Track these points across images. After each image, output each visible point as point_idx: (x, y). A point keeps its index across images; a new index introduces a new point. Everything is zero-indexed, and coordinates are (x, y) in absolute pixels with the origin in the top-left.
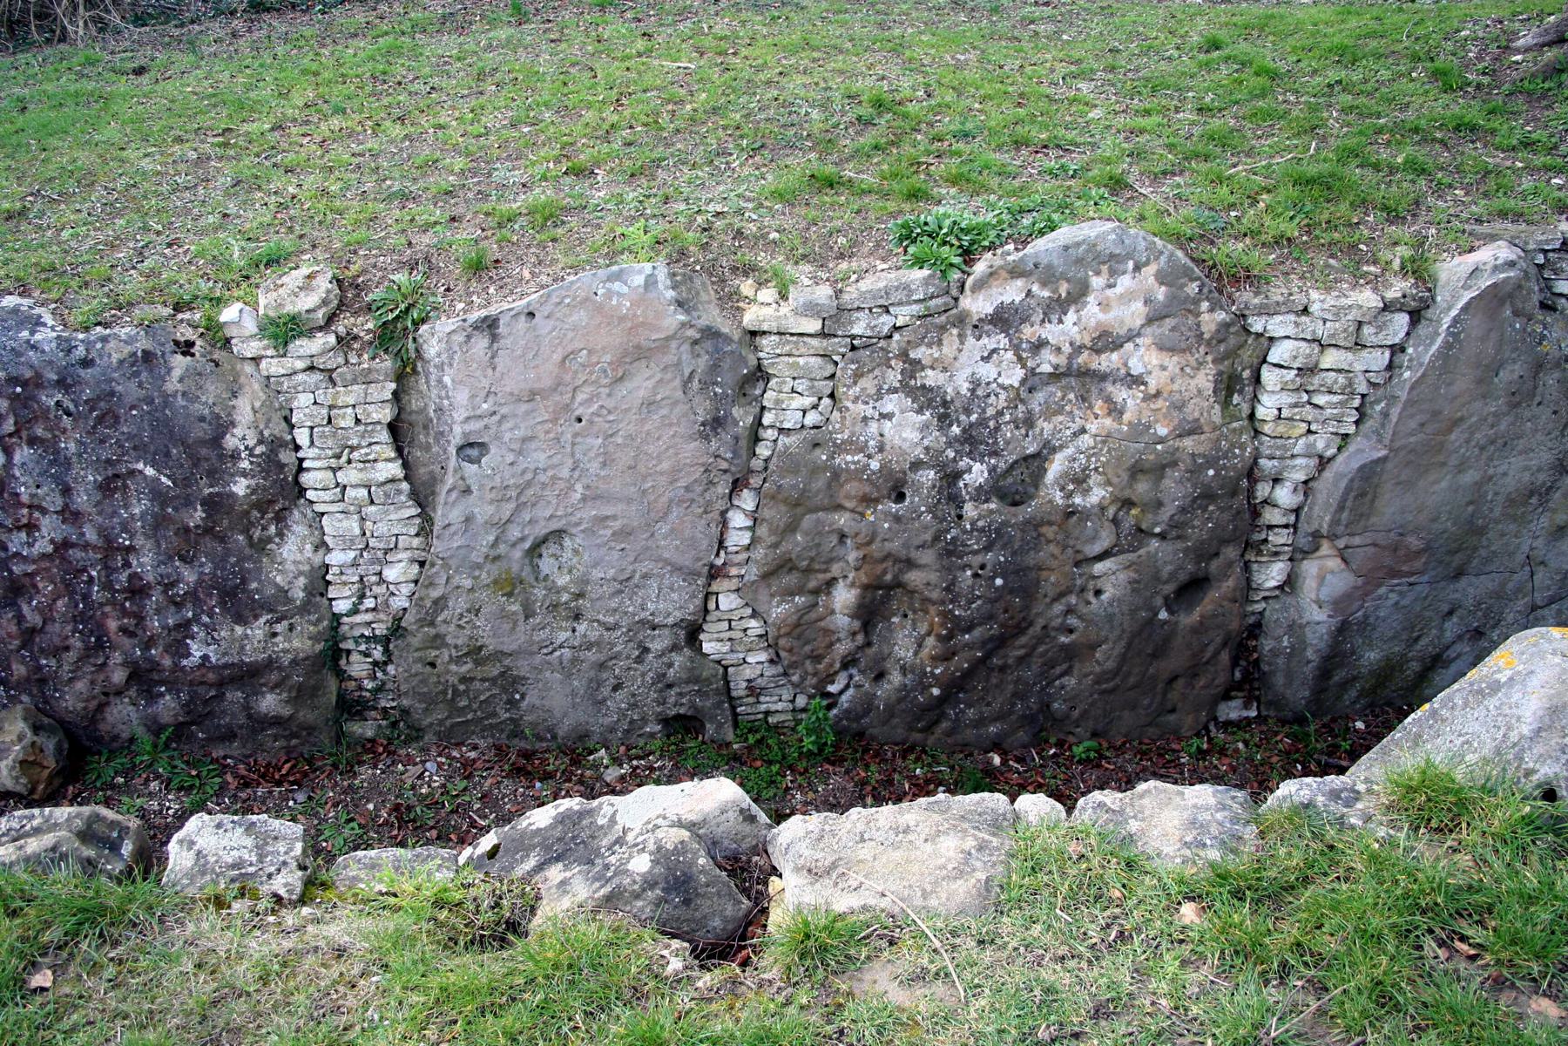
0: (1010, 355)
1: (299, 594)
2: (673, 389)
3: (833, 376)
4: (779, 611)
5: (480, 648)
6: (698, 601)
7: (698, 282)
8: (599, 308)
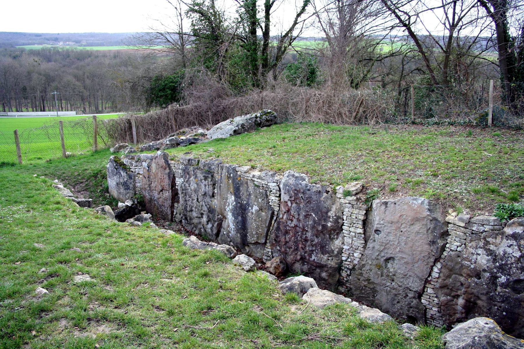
0: (516, 247)
1: (336, 252)
2: (424, 230)
3: (466, 239)
4: (443, 298)
5: (370, 280)
6: (422, 287)
7: (438, 206)
8: (410, 206)
